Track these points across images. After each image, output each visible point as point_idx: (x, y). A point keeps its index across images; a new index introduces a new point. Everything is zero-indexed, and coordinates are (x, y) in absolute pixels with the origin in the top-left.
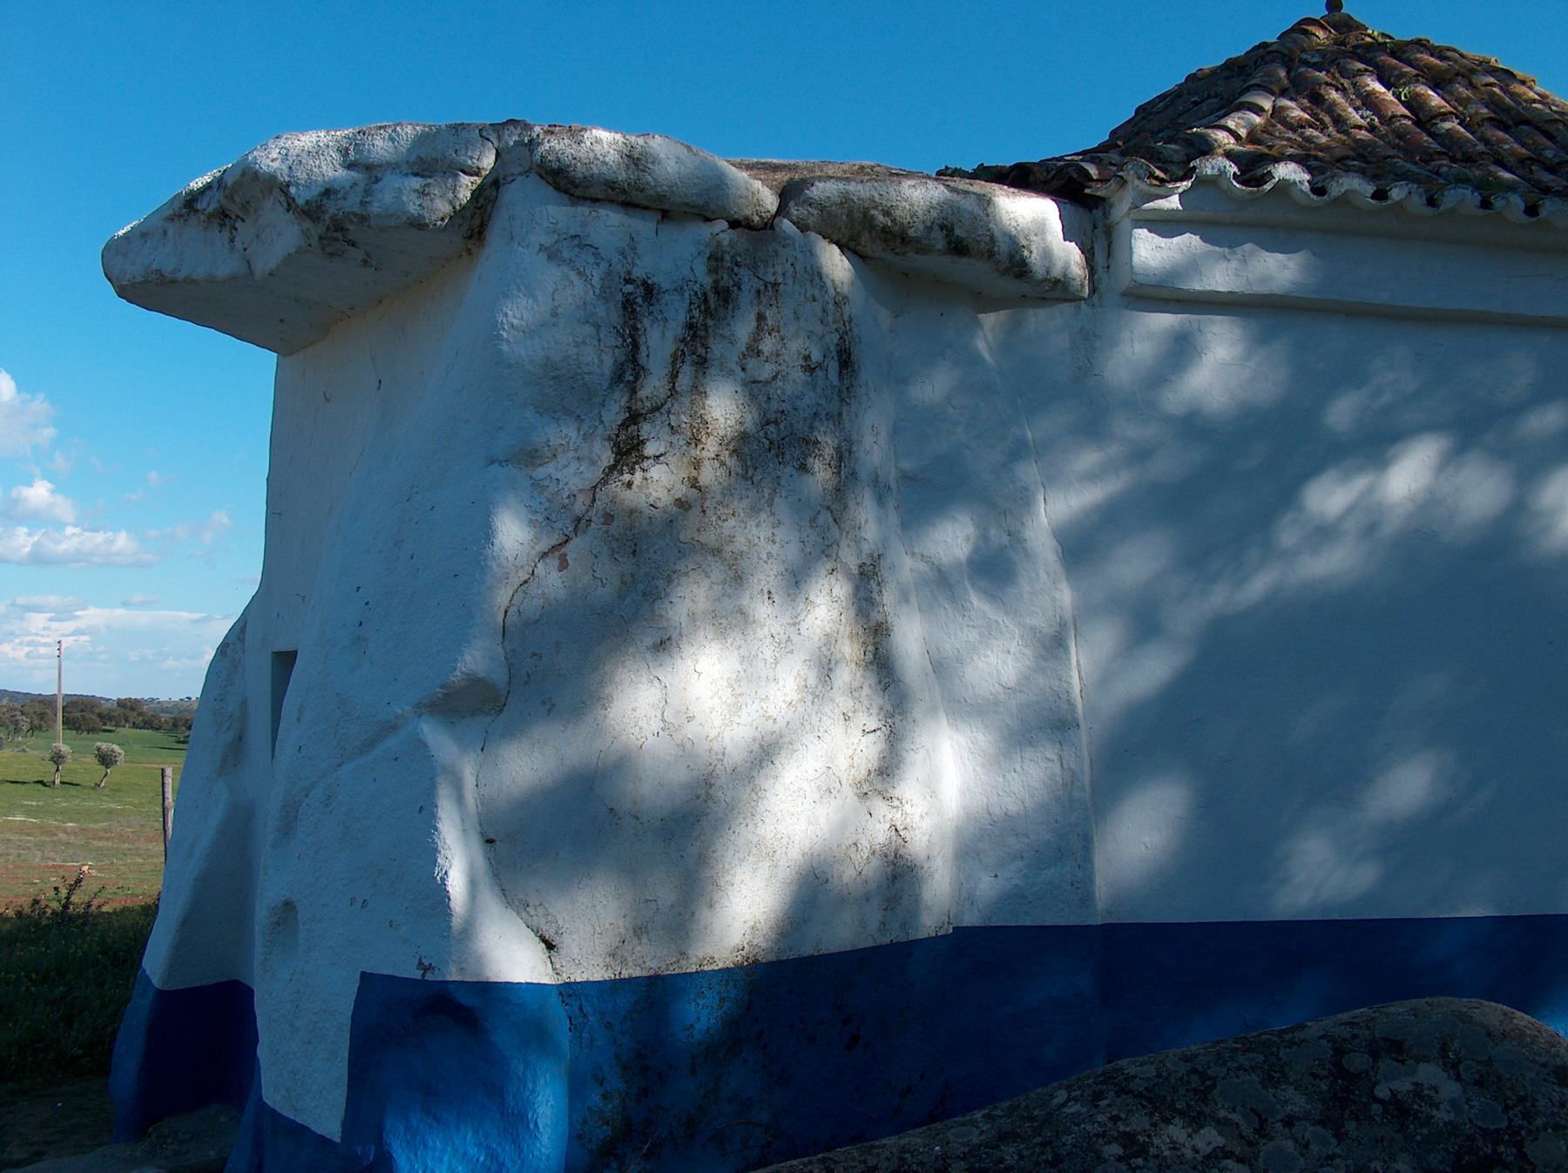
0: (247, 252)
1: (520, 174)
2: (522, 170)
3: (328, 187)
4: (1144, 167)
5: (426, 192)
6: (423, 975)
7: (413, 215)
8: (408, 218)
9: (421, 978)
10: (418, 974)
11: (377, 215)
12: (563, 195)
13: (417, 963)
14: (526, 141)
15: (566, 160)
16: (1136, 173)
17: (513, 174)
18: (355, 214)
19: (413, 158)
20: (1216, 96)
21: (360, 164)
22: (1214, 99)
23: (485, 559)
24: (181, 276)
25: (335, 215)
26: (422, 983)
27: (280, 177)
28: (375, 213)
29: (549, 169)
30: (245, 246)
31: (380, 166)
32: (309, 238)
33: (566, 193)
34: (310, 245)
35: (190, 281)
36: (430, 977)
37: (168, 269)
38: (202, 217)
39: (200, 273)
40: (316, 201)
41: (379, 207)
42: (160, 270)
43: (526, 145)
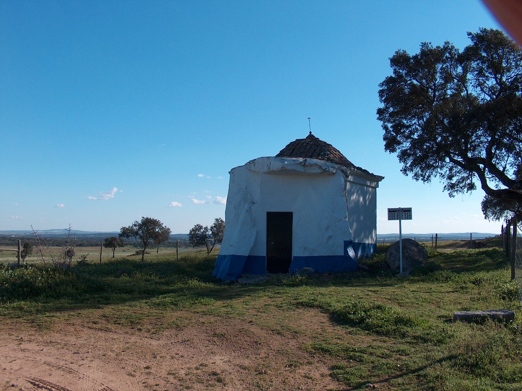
35: (298, 171)
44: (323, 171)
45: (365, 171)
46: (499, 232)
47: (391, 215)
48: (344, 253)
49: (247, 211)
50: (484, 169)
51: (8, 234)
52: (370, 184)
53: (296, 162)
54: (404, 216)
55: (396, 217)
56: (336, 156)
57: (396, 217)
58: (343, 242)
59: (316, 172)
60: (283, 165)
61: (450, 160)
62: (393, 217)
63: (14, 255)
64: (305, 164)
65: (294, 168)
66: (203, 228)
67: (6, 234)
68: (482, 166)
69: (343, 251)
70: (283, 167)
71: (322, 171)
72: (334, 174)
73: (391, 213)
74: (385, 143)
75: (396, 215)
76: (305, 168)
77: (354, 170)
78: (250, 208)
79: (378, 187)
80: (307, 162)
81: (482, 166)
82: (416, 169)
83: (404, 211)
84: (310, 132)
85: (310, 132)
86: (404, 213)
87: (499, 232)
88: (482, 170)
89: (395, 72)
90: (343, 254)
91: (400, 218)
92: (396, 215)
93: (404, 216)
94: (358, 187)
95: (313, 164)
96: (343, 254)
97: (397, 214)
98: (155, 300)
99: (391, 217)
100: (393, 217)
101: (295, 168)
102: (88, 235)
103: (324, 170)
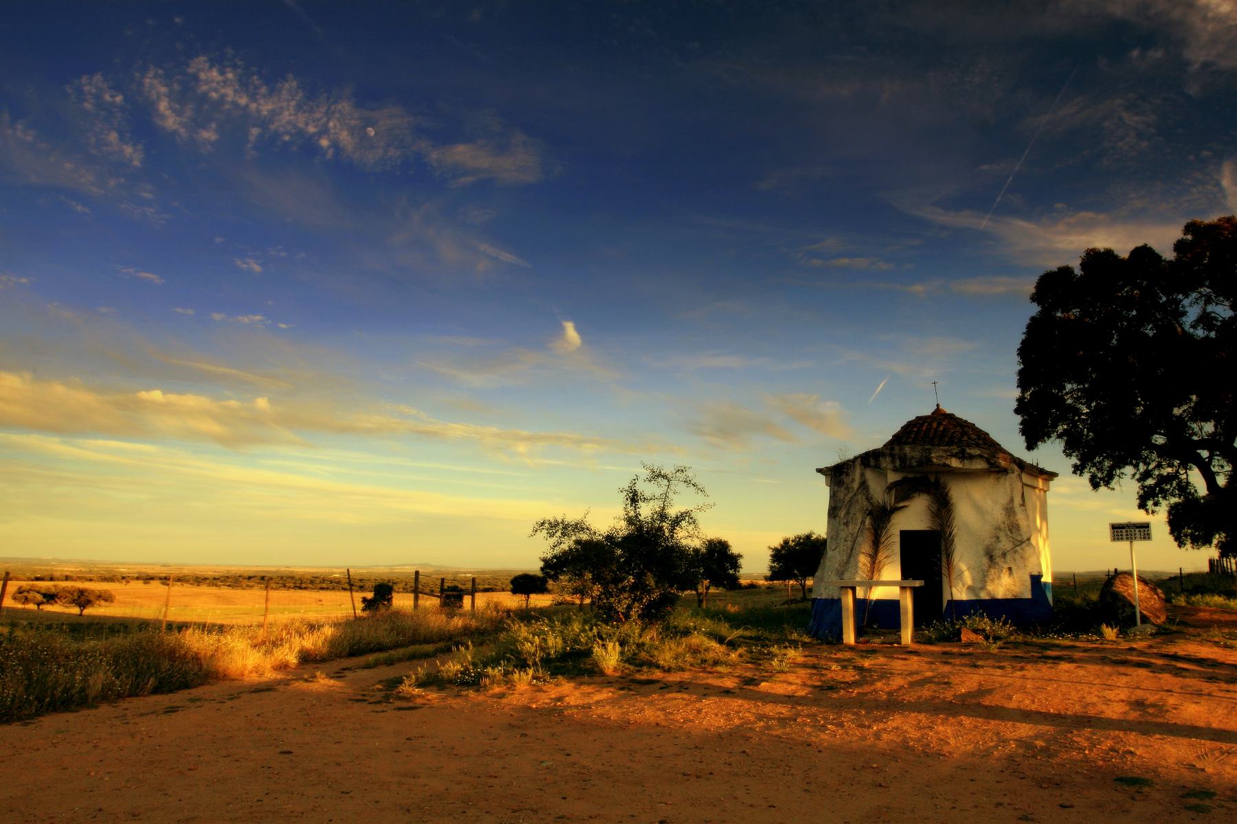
46: (1205, 568)
47: (1116, 534)
50: (1211, 458)
52: (866, 593)
54: (1138, 535)
55: (1124, 537)
57: (1124, 537)
61: (859, 600)
62: (1120, 537)
66: (174, 626)
68: (1205, 454)
73: (1115, 530)
74: (1019, 418)
75: (1124, 534)
81: (1205, 454)
82: (469, 789)
83: (1137, 527)
84: (938, 405)
85: (938, 405)
86: (1137, 530)
87: (1205, 568)
88: (1207, 460)
89: (1060, 436)
91: (1131, 538)
92: (1124, 534)
93: (1138, 535)
97: (1127, 531)
98: (919, 677)
99: (1116, 537)
100: (1120, 537)
102: (947, 549)
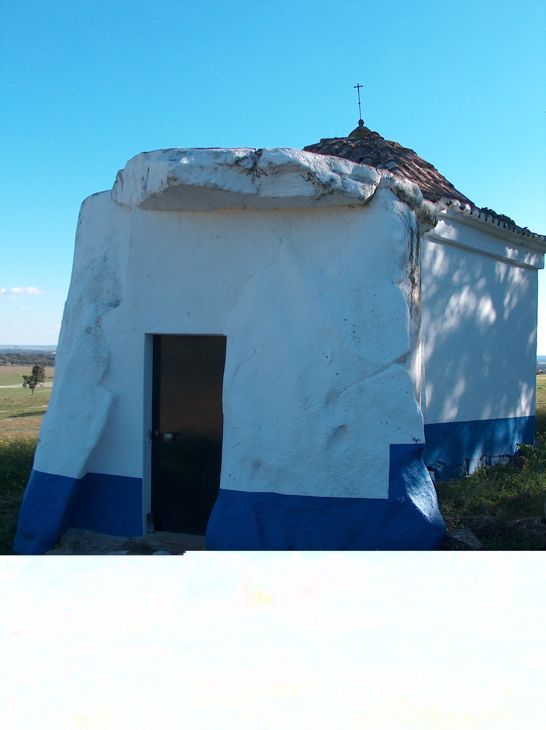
0: (260, 186)
1: (384, 187)
2: (385, 186)
3: (332, 178)
4: (446, 201)
5: (365, 188)
6: (416, 443)
7: (362, 195)
8: (360, 196)
9: (415, 443)
10: (414, 442)
11: (348, 192)
12: (398, 198)
13: (412, 439)
14: (390, 178)
15: (404, 188)
16: (444, 202)
17: (381, 187)
18: (340, 190)
19: (354, 174)
20: (371, 158)
21: (337, 171)
22: (370, 159)
23: (406, 315)
24: (226, 188)
25: (334, 188)
26: (416, 445)
27: (312, 169)
28: (348, 191)
29: (399, 189)
30: (261, 184)
31: (345, 174)
32: (317, 193)
33: (399, 197)
34: (316, 195)
35: (228, 191)
36: (418, 443)
37: (220, 184)
38: (242, 168)
39: (235, 189)
40: (329, 182)
41: (350, 190)
42: (216, 184)
43: (389, 179)
44: (321, 190)
45: (504, 219)
48: (391, 492)
49: (88, 330)
51: (47, 350)
53: (220, 161)
56: (421, 176)
58: (389, 445)
59: (294, 192)
60: (171, 168)
63: (50, 379)
64: (255, 164)
65: (213, 181)
67: (45, 349)
69: (386, 484)
70: (171, 175)
71: (316, 192)
72: (368, 202)
76: (258, 181)
77: (462, 208)
78: (98, 321)
79: (543, 268)
80: (262, 158)
84: (361, 122)
85: (361, 122)
90: (384, 495)
94: (479, 264)
95: (283, 165)
96: (384, 495)
101: (215, 179)
103: (325, 186)
